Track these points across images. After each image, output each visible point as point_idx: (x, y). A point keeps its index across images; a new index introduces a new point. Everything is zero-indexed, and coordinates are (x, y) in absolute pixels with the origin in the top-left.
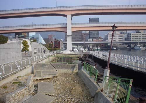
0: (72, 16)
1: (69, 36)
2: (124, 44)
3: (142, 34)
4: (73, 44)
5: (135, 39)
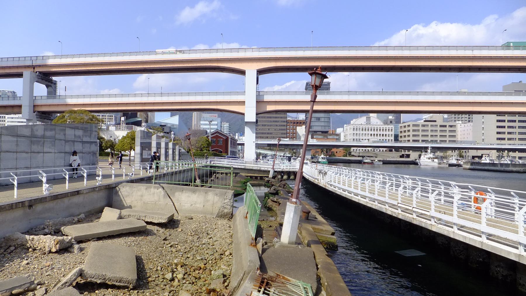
0: (257, 74)
1: (248, 123)
2: (391, 151)
3: (441, 126)
4: (258, 146)
5: (506, 124)
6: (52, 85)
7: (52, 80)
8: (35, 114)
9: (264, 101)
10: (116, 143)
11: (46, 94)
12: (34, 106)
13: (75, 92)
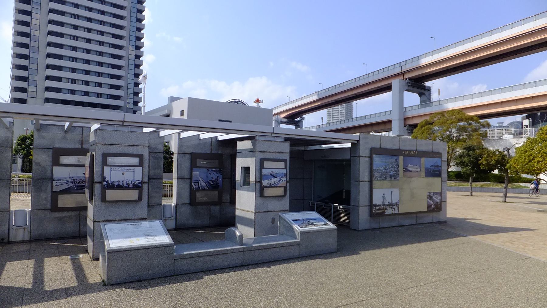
6: (426, 93)
7: (425, 86)
8: (406, 128)
9: (359, 231)
10: (510, 157)
11: (419, 103)
12: (405, 119)
13: (451, 95)
